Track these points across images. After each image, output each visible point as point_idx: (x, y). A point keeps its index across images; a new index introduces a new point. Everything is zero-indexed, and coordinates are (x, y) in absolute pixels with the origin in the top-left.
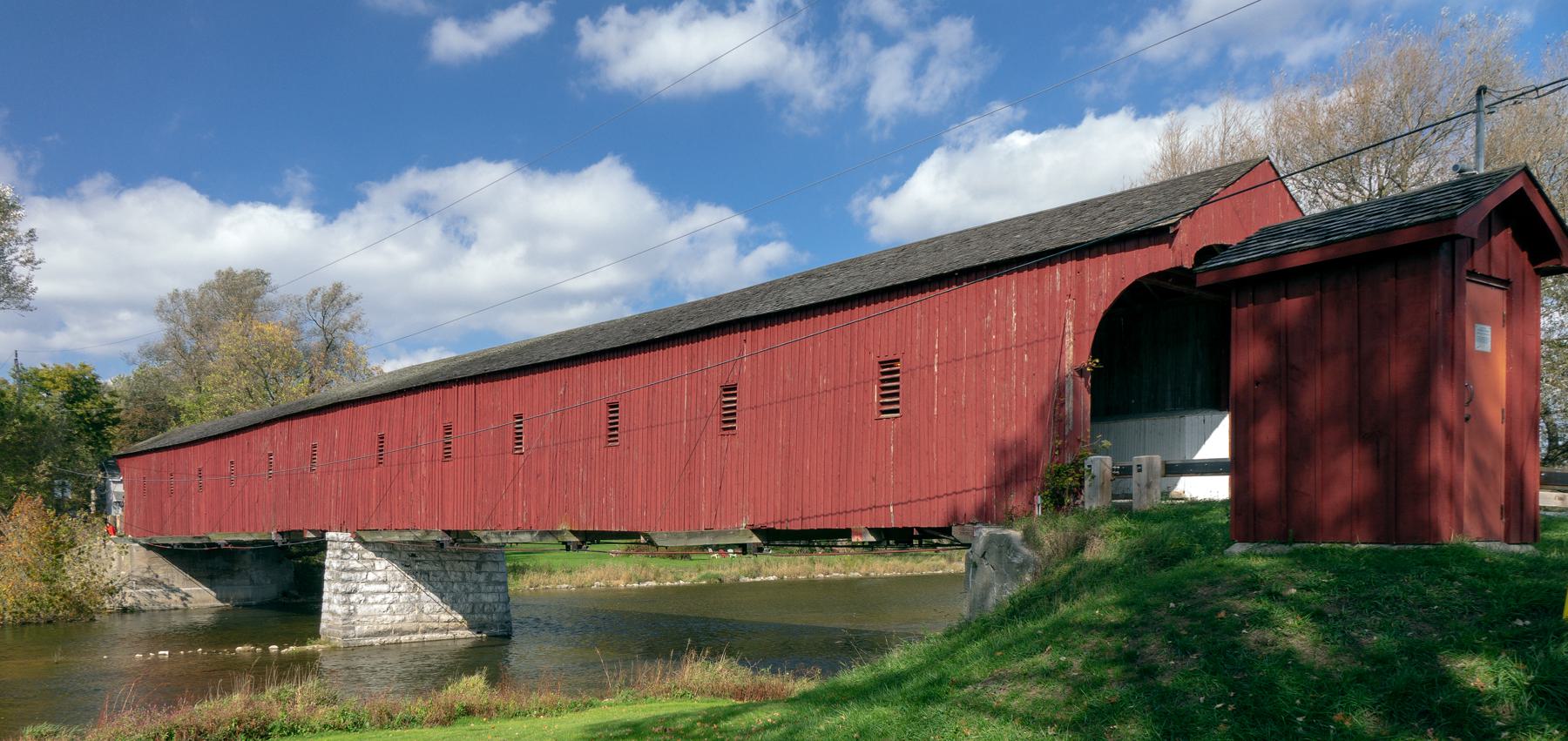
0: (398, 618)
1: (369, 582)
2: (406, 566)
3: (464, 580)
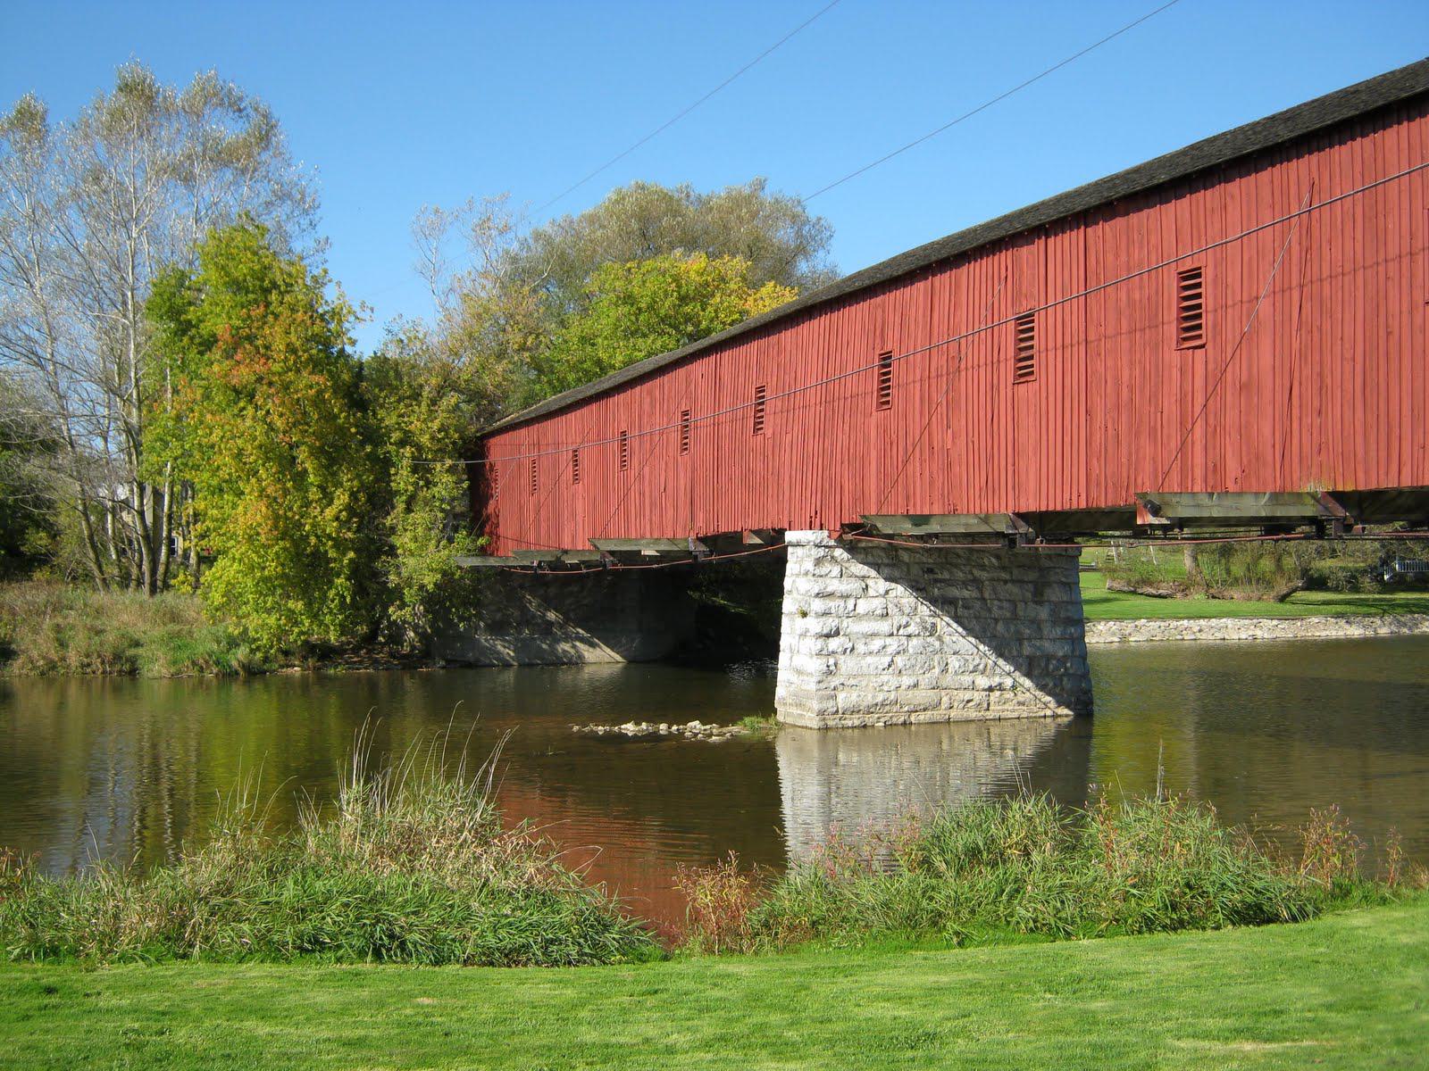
0: (907, 681)
1: (859, 617)
2: (919, 588)
3: (1015, 617)
